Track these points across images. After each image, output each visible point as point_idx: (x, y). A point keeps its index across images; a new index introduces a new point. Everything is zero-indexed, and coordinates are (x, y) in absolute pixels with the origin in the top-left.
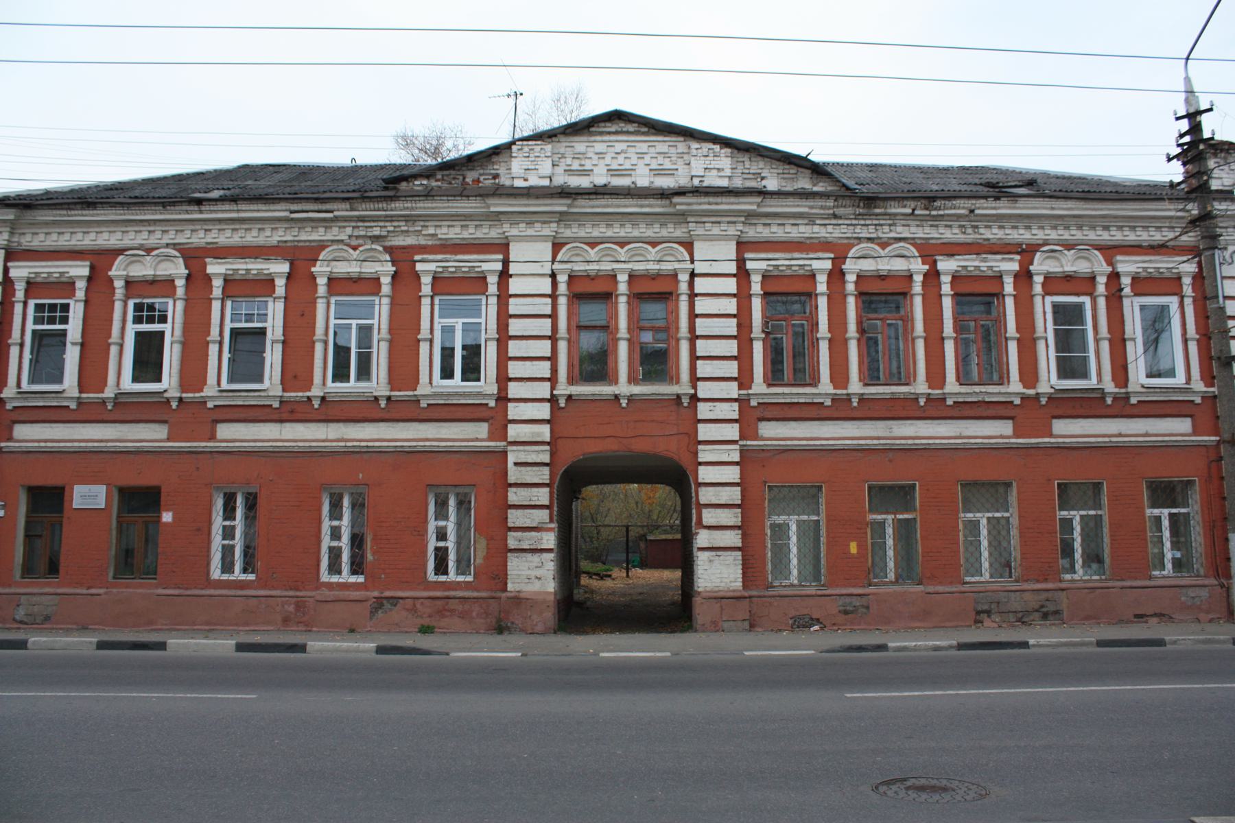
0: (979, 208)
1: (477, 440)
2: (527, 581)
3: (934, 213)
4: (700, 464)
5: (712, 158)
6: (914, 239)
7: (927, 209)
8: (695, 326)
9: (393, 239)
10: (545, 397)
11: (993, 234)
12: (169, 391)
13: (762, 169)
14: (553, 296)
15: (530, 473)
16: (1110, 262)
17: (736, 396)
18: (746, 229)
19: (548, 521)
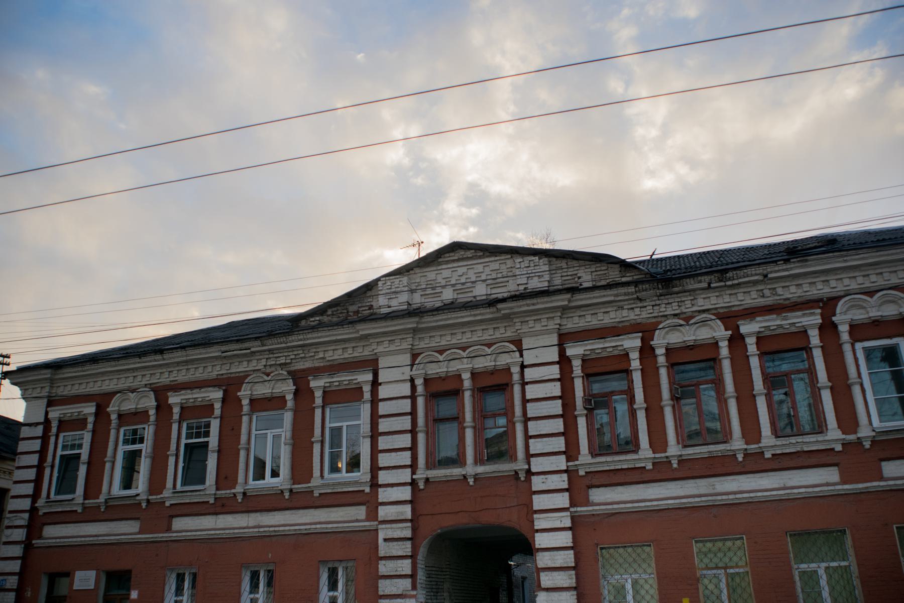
0: (771, 272)
1: (357, 521)
4: (537, 531)
5: (533, 268)
6: (716, 309)
7: (721, 281)
8: (526, 410)
9: (296, 364)
10: (407, 481)
11: (793, 292)
12: (141, 495)
14: (413, 397)
17: (565, 468)
18: (564, 322)
19: (410, 589)
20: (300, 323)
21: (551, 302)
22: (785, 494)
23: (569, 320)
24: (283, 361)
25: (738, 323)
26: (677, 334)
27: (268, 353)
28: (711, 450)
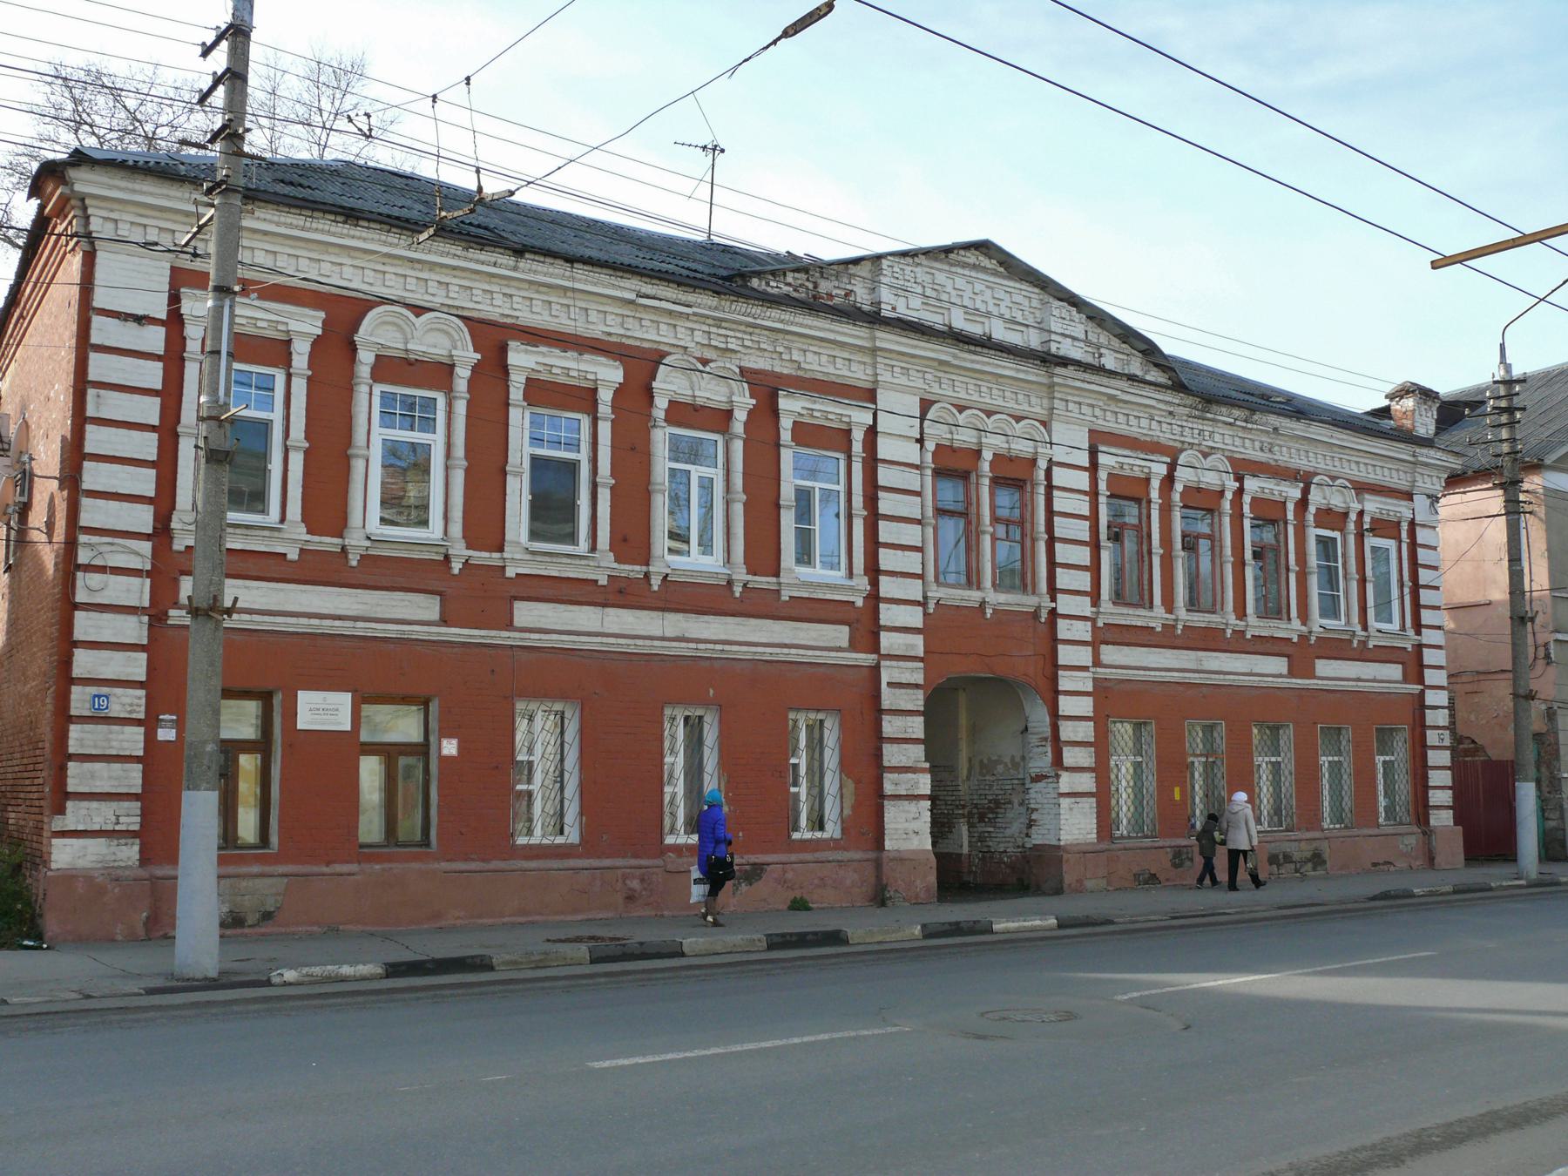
15: (905, 697)
16: (1239, 479)
21: (134, 191)
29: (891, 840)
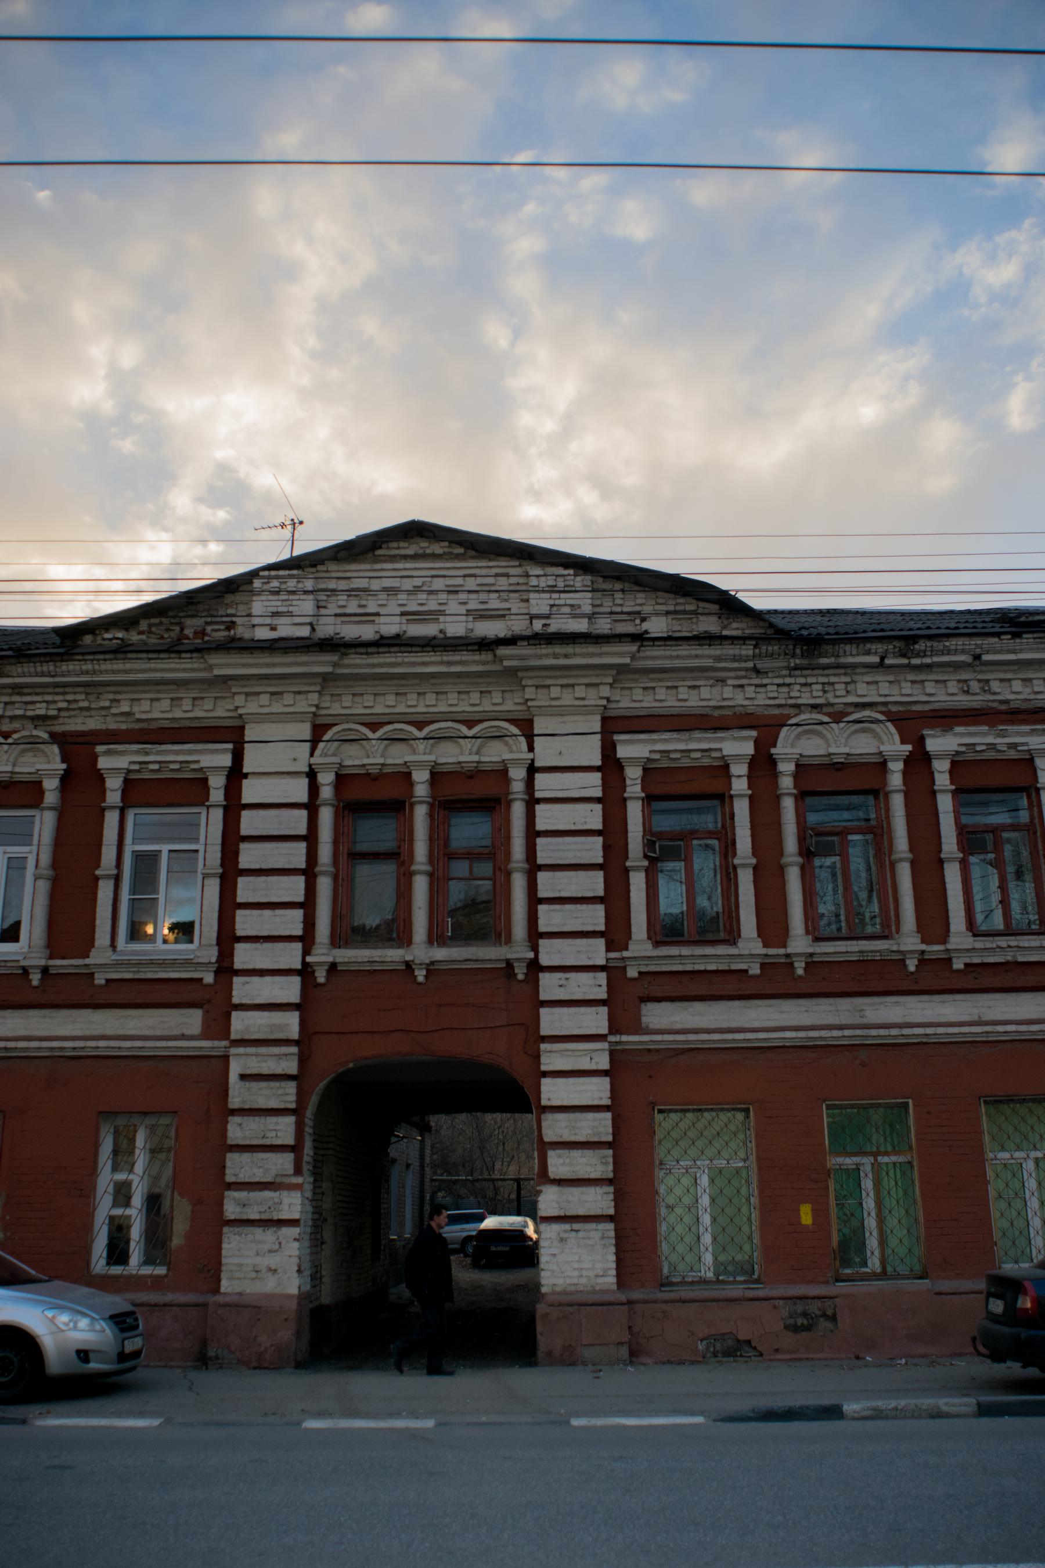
0: (988, 653)
1: (183, 1037)
2: (254, 1275)
3: (916, 661)
4: (545, 1074)
6: (885, 704)
7: (903, 655)
9: (67, 721)
10: (294, 967)
13: (641, 605)
14: (312, 807)
15: (265, 1092)
17: (602, 962)
19: (292, 1172)
20: (82, 640)
21: (600, 655)
22: (982, 1033)
23: (624, 692)
24: (42, 712)
25: (924, 733)
26: (817, 741)
27: (10, 691)
28: (864, 948)
29: (230, 1279)
